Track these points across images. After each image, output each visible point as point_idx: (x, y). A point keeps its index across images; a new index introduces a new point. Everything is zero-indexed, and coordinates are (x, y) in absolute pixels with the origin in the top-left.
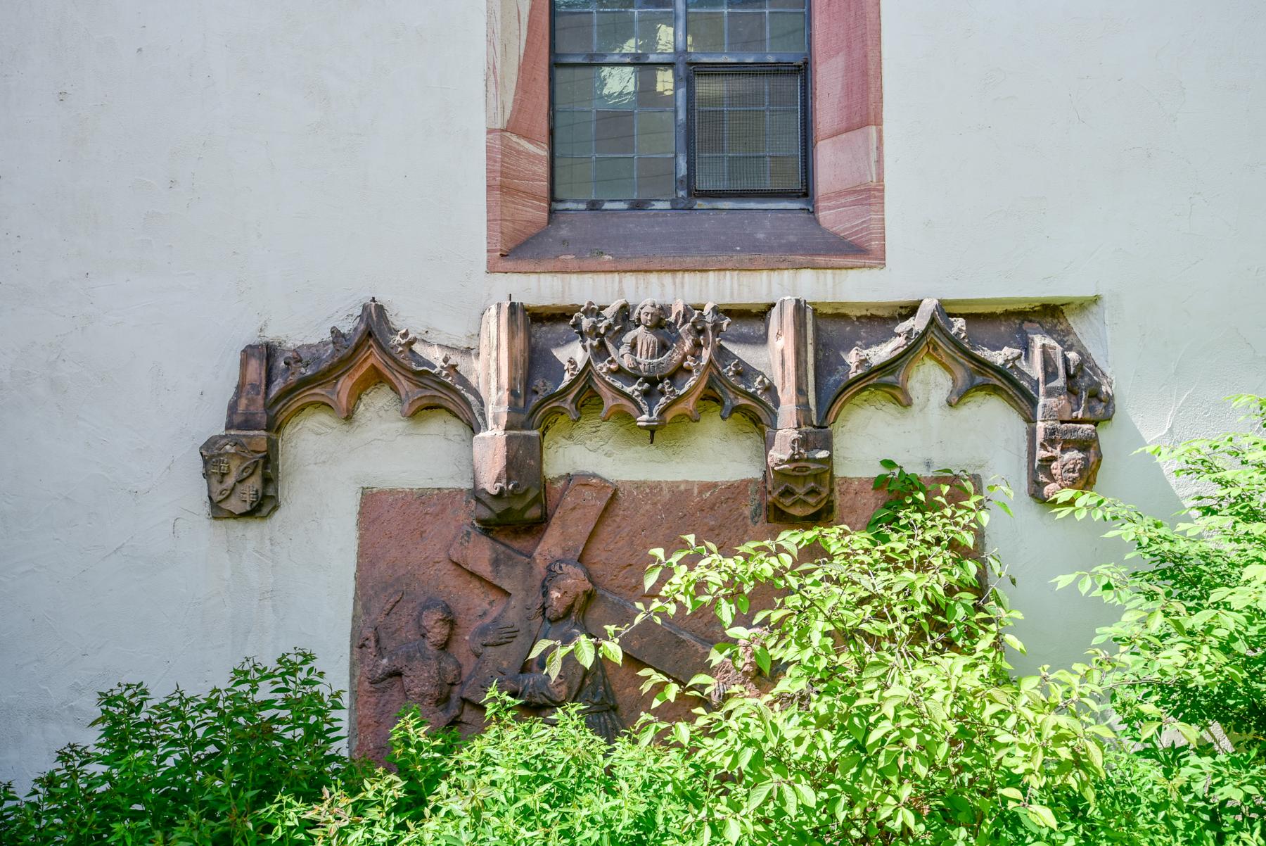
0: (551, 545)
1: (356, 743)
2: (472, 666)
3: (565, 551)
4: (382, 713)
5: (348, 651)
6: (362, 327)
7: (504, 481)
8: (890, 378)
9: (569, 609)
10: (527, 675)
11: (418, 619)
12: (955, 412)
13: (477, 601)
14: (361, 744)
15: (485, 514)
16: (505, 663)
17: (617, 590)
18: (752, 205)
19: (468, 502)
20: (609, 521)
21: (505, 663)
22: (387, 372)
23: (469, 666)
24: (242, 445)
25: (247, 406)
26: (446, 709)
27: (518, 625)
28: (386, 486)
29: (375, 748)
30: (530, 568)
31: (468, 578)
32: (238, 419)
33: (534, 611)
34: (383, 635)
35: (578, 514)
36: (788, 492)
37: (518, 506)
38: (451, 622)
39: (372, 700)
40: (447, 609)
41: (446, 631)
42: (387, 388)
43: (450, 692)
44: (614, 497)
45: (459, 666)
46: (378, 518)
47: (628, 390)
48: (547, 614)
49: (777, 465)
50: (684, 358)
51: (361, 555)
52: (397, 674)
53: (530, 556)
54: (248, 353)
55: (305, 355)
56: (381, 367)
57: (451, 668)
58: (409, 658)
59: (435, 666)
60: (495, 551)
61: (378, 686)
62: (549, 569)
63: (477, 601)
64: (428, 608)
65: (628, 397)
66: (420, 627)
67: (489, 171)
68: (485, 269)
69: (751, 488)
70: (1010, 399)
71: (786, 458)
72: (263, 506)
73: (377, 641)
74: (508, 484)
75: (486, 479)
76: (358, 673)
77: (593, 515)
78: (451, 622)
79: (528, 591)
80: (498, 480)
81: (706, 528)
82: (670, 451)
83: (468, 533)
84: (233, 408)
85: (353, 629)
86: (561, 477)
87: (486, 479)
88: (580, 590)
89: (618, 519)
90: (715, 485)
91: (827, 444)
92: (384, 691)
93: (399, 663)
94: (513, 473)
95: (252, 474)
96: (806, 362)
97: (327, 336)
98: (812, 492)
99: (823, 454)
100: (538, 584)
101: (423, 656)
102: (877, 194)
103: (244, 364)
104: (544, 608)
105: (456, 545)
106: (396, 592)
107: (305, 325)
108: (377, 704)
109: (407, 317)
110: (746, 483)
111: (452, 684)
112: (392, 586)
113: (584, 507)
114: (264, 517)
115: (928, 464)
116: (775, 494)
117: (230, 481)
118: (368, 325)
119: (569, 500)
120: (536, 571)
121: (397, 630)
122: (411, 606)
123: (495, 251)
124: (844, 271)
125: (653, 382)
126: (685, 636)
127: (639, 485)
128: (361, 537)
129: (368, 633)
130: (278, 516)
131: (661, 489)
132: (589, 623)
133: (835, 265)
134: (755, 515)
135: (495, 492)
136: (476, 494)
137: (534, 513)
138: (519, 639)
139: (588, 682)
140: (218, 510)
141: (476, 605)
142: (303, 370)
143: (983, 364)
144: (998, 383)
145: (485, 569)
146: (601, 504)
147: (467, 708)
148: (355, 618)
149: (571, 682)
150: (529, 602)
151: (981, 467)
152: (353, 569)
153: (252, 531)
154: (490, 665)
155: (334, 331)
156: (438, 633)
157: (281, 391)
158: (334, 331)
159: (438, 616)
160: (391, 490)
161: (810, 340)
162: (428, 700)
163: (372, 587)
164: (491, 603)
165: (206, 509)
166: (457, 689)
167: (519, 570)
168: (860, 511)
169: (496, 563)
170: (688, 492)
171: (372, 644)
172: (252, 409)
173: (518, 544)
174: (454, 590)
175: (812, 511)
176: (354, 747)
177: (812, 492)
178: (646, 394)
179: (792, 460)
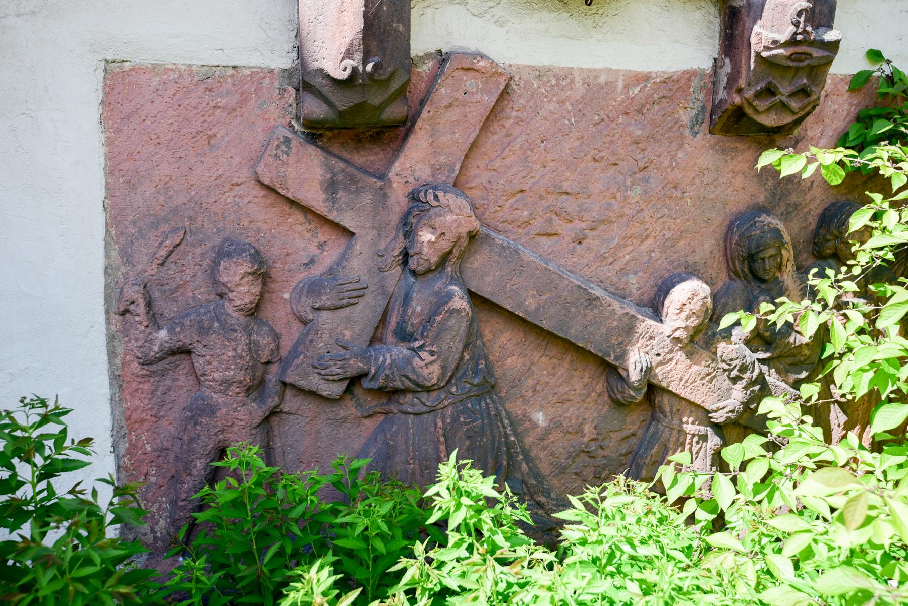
0: (414, 161)
1: (124, 446)
2: (296, 336)
3: (435, 170)
4: (162, 404)
5: (102, 318)
7: (359, 56)
9: (445, 259)
11: (213, 272)
13: (299, 243)
15: (315, 109)
16: (348, 333)
17: (501, 227)
21: (348, 333)
23: (291, 334)
26: (261, 399)
27: (365, 278)
28: (146, 58)
29: (154, 450)
30: (383, 195)
31: (286, 208)
34: (156, 295)
35: (453, 115)
36: (769, 91)
37: (376, 99)
38: (263, 275)
39: (146, 387)
40: (257, 257)
41: (256, 290)
43: (265, 372)
44: (505, 94)
45: (277, 337)
46: (134, 113)
48: (413, 263)
49: (767, 48)
51: (111, 171)
53: (382, 176)
57: (265, 341)
58: (203, 331)
59: (244, 340)
60: (330, 169)
61: (154, 367)
62: (414, 197)
63: (299, 243)
64: (228, 255)
69: (695, 83)
71: (783, 38)
73: (149, 304)
74: (365, 62)
75: (324, 53)
76: (120, 350)
77: (477, 114)
78: (263, 275)
79: (380, 229)
80: (348, 54)
82: (589, 21)
83: (287, 140)
85: (107, 286)
86: (428, 56)
87: (324, 53)
89: (508, 124)
90: (647, 77)
92: (163, 373)
93: (186, 338)
94: (374, 44)
100: (395, 219)
101: (223, 326)
104: (406, 256)
105: (268, 159)
106: (174, 230)
108: (153, 393)
110: (689, 75)
111: (268, 363)
112: (166, 220)
116: (749, 94)
119: (443, 91)
120: (392, 200)
121: (179, 287)
122: (199, 250)
126: (598, 292)
127: (540, 73)
128: (109, 142)
129: (133, 293)
131: (572, 81)
132: (468, 274)
134: (696, 122)
135: (344, 75)
136: (305, 80)
137: (395, 112)
138: (369, 299)
141: (299, 248)
145: (315, 197)
146: (489, 100)
147: (288, 393)
149: (446, 360)
150: (382, 246)
152: (101, 194)
154: (326, 336)
156: (245, 293)
159: (246, 267)
160: (155, 67)
162: (234, 389)
163: (134, 223)
164: (321, 246)
166: (274, 368)
167: (367, 198)
168: (827, 121)
169: (331, 187)
170: (610, 85)
171: (141, 308)
173: (360, 158)
174: (265, 227)
179: (792, 42)
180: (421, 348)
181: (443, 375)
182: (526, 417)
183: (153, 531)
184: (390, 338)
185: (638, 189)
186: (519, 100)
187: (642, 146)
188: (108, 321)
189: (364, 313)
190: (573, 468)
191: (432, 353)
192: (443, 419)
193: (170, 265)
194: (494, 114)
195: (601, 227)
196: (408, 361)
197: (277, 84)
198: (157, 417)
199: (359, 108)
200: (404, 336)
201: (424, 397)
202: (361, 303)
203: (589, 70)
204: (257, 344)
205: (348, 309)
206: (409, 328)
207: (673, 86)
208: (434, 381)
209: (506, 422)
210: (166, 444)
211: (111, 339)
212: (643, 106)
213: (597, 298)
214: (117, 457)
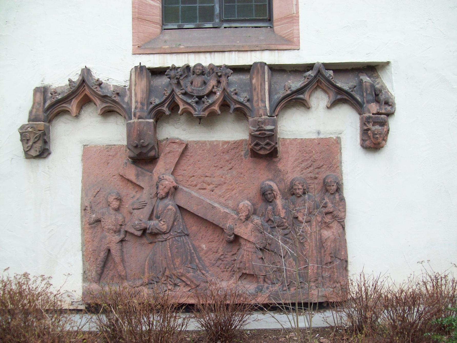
1: (84, 249)
5: (80, 211)
6: (81, 78)
8: (301, 96)
10: (151, 221)
12: (329, 111)
14: (87, 249)
18: (247, 25)
19: (126, 150)
20: (184, 158)
21: (142, 217)
22: (91, 97)
24: (34, 128)
25: (36, 112)
26: (119, 235)
30: (151, 177)
31: (127, 182)
32: (32, 117)
33: (153, 195)
36: (257, 144)
37: (145, 151)
39: (90, 231)
42: (93, 104)
43: (120, 228)
44: (186, 148)
47: (189, 101)
50: (213, 87)
52: (98, 221)
54: (37, 90)
55: (59, 91)
56: (89, 94)
59: (114, 217)
61: (92, 226)
62: (159, 178)
65: (189, 104)
66: (108, 202)
67: (133, 12)
68: (132, 53)
69: (244, 143)
70: (352, 105)
72: (44, 153)
73: (91, 207)
76: (84, 220)
78: (120, 200)
81: (225, 160)
84: (31, 112)
85: (81, 203)
86: (164, 140)
88: (172, 186)
91: (275, 123)
93: (99, 216)
95: (39, 140)
96: (265, 89)
97: (68, 83)
98: (268, 144)
99: (272, 127)
102: (296, 18)
103: (35, 95)
104: (157, 194)
107: (60, 78)
108: (92, 233)
109: (99, 74)
110: (242, 141)
111: (121, 225)
113: (174, 152)
114: (45, 158)
115: (319, 133)
117: (30, 143)
118: (83, 77)
119: (168, 149)
121: (99, 203)
122: (104, 193)
123: (136, 45)
124: (282, 51)
125: (200, 98)
127: (197, 142)
128: (83, 166)
130: (51, 157)
131: (206, 144)
133: (279, 49)
137: (152, 153)
139: (175, 224)
140: (28, 156)
142: (57, 96)
143: (340, 90)
144: (346, 98)
145: (133, 178)
146: (180, 150)
148: (82, 198)
151: (341, 133)
152: (81, 178)
153: (42, 164)
155: (70, 81)
157: (54, 107)
158: (70, 81)
161: (266, 79)
165: (23, 154)
166: (123, 227)
169: (137, 176)
172: (38, 113)
175: (268, 152)
176: (84, 250)
177: (268, 144)
178: (197, 103)
180: (161, 220)
181: (168, 228)
182: (200, 247)
183: (91, 275)
184: (154, 218)
185: (229, 175)
186: (191, 149)
187: (229, 162)
188: (81, 212)
189: (147, 211)
190: (217, 265)
191: (164, 222)
192: (169, 243)
193: (97, 197)
194: (183, 154)
195: (219, 187)
196: (157, 224)
197: (125, 149)
198: (93, 241)
199: (140, 154)
200: (158, 218)
201: (163, 236)
202: (146, 208)
203: (211, 141)
204: (118, 219)
205: (142, 209)
206: (159, 215)
207: (237, 145)
208: (165, 230)
209: (191, 246)
210: (95, 249)
211: (82, 217)
212: (229, 150)
213: (215, 207)
214: (83, 252)
